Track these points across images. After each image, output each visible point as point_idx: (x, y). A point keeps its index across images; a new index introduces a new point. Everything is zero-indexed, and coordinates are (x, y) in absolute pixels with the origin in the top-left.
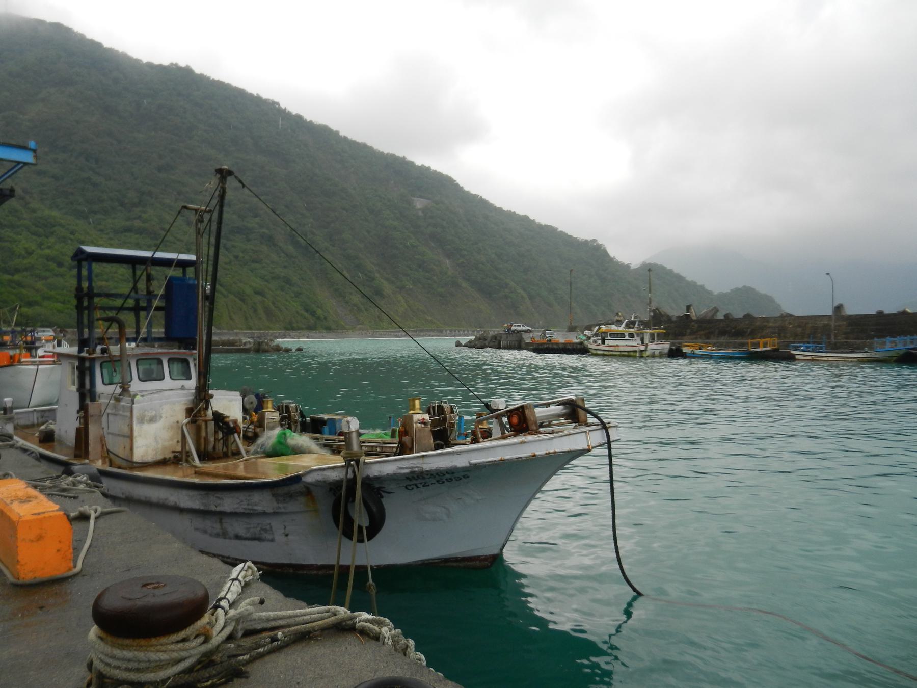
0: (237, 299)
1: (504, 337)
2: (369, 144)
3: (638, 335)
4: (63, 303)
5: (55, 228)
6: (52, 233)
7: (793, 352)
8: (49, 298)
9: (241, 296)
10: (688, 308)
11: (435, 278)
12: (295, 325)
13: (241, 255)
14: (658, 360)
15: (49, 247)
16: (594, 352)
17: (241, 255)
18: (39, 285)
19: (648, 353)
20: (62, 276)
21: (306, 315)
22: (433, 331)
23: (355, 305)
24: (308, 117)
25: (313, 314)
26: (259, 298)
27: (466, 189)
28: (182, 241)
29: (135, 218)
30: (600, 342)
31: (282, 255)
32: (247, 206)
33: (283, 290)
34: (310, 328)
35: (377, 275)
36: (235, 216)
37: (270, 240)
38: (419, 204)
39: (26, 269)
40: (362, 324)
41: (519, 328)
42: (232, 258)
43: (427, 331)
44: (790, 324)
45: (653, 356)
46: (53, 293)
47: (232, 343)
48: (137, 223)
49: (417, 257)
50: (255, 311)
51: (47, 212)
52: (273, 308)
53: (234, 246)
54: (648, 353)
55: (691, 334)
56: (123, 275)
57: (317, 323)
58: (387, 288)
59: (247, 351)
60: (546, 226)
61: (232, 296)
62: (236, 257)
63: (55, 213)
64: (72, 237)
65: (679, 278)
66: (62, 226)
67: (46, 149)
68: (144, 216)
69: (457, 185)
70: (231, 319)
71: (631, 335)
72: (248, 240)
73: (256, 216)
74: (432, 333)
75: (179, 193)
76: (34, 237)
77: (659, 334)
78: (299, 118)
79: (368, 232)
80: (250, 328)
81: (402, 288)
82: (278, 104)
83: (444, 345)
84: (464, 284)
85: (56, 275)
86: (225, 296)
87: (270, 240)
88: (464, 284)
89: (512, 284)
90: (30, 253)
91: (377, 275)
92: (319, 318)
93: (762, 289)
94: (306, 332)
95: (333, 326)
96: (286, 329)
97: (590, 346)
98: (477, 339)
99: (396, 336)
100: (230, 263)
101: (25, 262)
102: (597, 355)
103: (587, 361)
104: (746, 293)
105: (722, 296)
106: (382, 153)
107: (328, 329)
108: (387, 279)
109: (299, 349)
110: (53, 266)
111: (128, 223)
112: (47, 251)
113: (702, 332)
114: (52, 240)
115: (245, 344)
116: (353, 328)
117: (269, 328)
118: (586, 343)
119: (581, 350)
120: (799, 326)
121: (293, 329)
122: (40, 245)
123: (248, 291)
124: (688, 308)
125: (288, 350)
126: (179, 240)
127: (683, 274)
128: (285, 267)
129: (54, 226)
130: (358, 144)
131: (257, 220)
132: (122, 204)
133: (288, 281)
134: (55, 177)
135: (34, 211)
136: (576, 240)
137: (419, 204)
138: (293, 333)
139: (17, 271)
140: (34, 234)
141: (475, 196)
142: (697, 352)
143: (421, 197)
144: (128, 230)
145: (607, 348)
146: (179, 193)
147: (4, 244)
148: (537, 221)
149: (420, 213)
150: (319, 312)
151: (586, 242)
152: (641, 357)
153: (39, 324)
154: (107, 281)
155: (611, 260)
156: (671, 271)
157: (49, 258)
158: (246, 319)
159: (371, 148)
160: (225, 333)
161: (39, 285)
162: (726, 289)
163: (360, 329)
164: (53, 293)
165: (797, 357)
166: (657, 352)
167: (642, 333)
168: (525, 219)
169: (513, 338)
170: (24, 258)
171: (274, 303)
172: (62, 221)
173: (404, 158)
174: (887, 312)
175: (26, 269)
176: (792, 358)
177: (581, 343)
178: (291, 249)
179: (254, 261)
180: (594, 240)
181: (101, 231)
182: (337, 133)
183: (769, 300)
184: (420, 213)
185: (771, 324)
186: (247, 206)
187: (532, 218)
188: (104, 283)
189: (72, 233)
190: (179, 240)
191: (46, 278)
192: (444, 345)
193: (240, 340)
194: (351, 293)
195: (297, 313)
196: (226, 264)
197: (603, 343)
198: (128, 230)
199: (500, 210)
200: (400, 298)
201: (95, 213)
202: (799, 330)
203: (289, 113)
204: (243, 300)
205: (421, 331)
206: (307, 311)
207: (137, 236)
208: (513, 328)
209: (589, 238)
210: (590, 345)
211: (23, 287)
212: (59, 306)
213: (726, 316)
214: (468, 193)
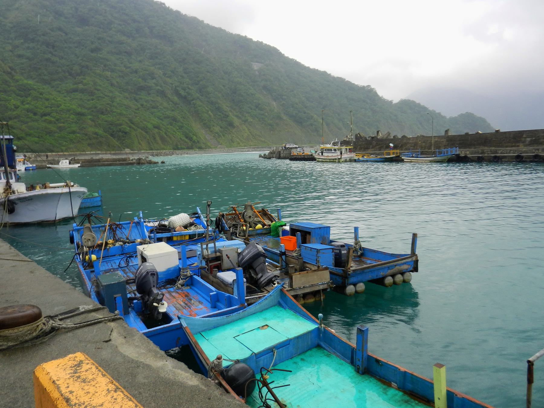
0: (143, 132)
1: (282, 152)
2: (223, 28)
3: (338, 150)
4: (38, 137)
5: (31, 91)
6: (29, 95)
7: (403, 158)
8: (30, 135)
9: (145, 129)
10: (378, 132)
11: (266, 114)
12: (179, 147)
13: (145, 104)
14: (349, 163)
15: (28, 104)
16: (318, 160)
17: (145, 104)
18: (24, 127)
19: (342, 160)
20: (37, 121)
21: (186, 140)
22: (265, 147)
23: (217, 133)
24: (183, 12)
25: (191, 139)
26: (157, 130)
27: (286, 55)
28: (108, 96)
29: (79, 83)
30: (320, 154)
31: (171, 103)
32: (147, 72)
33: (171, 125)
34: (190, 148)
35: (230, 114)
36: (140, 79)
37: (162, 94)
38: (256, 66)
39: (15, 118)
40: (221, 144)
41: (290, 146)
42: (139, 106)
43: (262, 147)
44: (420, 141)
45: (346, 161)
46: (32, 131)
47: (124, 160)
48: (81, 86)
49: (255, 101)
50: (155, 138)
51: (25, 81)
52: (166, 136)
53: (141, 99)
54: (342, 160)
55: (372, 148)
56: (73, 119)
57: (192, 144)
58: (237, 122)
59: (132, 164)
60: (338, 78)
61: (139, 130)
62: (142, 105)
63: (30, 82)
64: (41, 96)
65: (424, 109)
66: (34, 89)
67: (22, 41)
68: (85, 81)
69: (280, 53)
70: (140, 144)
71: (335, 150)
72: (149, 94)
73: (153, 79)
74: (265, 149)
75: (105, 66)
76: (19, 98)
77: (350, 149)
78: (178, 12)
79: (224, 86)
80: (152, 149)
81: (246, 121)
82: (164, 4)
83: (250, 156)
84: (285, 117)
85: (34, 121)
86: (135, 130)
87: (162, 94)
88: (285, 117)
89: (315, 116)
90: (17, 107)
91: (230, 114)
92: (194, 142)
93: (478, 114)
94: (185, 151)
95: (203, 146)
96: (174, 149)
97: (316, 157)
98: (271, 153)
99: (242, 151)
100: (138, 109)
101: (14, 113)
102: (319, 161)
103: (318, 167)
104: (468, 117)
105: (454, 120)
106: (232, 34)
107: (200, 148)
108: (237, 116)
109: (163, 162)
110: (31, 115)
111: (75, 86)
112: (27, 106)
113: (378, 147)
114: (29, 99)
115: (132, 160)
116: (216, 148)
117: (163, 149)
118: (314, 155)
119: (311, 158)
120: (424, 142)
121: (178, 149)
122: (22, 102)
123: (150, 126)
124: (378, 132)
125: (155, 163)
126: (106, 96)
127: (426, 105)
128: (173, 110)
129: (30, 90)
130: (216, 28)
131: (154, 81)
132: (71, 74)
133: (175, 119)
134: (28, 58)
135: (17, 81)
136: (357, 86)
137: (256, 66)
138: (177, 152)
139: (10, 119)
140: (18, 95)
141: (292, 60)
142: (361, 159)
143: (257, 62)
144: (75, 90)
145: (323, 158)
146: (105, 66)
147: (1, 102)
148: (332, 75)
149: (257, 73)
150: (194, 138)
151: (363, 87)
152: (339, 162)
153: (25, 150)
154: (64, 123)
155: (380, 99)
156: (419, 104)
157: (28, 110)
158: (149, 143)
159: (224, 31)
160: (99, 154)
161: (24, 127)
162: (455, 115)
163: (220, 148)
164: (32, 131)
165: (405, 160)
166: (348, 159)
167: (341, 149)
168: (324, 73)
169: (286, 152)
170: (14, 111)
171: (166, 133)
172: (35, 87)
173: (246, 36)
174: (502, 130)
175: (15, 118)
176: (402, 161)
177: (312, 155)
178: (176, 99)
179: (153, 108)
180: (369, 86)
181: (59, 92)
182: (203, 21)
183: (484, 120)
184: (257, 73)
185: (411, 141)
186: (147, 72)
187: (329, 73)
188: (62, 124)
189: (41, 94)
190: (106, 96)
191: (27, 123)
192: (250, 156)
193: (129, 158)
194: (214, 126)
195: (181, 139)
196: (136, 109)
197: (322, 154)
198: (75, 90)
199: (308, 69)
200: (244, 127)
201: (55, 80)
202: (424, 144)
203: (171, 10)
204: (147, 132)
205: (258, 148)
206: (187, 138)
207: (80, 94)
208: (287, 146)
209: (366, 85)
210: (316, 156)
211: (14, 128)
212: (36, 139)
213: (394, 137)
214: (287, 58)
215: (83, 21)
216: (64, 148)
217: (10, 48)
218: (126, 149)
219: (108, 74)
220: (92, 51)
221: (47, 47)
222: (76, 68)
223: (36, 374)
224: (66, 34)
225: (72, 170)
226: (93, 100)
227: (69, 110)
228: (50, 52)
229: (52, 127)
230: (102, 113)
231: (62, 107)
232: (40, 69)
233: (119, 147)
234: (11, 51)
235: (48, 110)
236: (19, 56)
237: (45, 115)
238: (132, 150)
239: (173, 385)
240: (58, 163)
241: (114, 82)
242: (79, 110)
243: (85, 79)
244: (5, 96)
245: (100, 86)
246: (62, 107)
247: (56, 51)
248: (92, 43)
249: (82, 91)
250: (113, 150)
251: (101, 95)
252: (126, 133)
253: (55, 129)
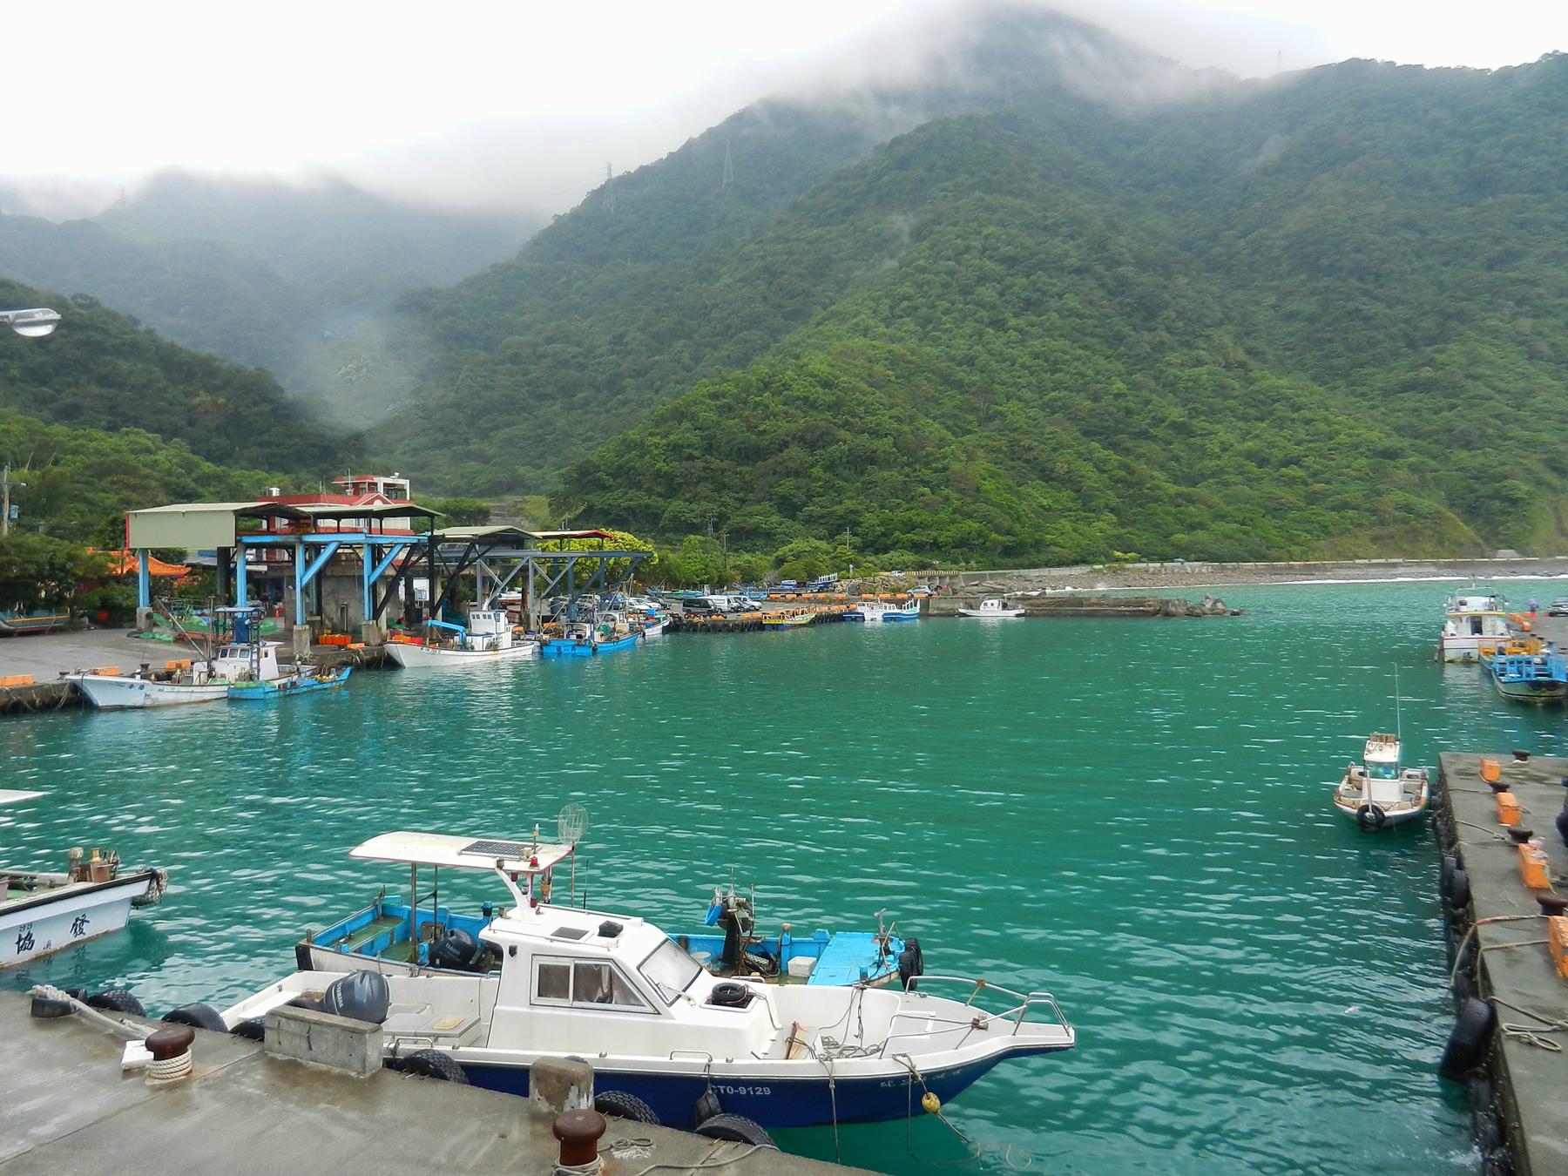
8: (1223, 517)
39: (1213, 474)
46: (1230, 509)
48: (1427, 372)
67: (1303, 277)
68: (1441, 358)
110: (1251, 466)
126: (1500, 392)
146: (1519, 303)
164: (1230, 509)
190: (1500, 392)
215: (1480, 185)
216: (1295, 549)
217: (1272, 300)
218: (1502, 552)
219: (1525, 324)
220: (1491, 266)
221: (1361, 280)
222: (1428, 323)
223: (640, 919)
224: (1423, 233)
225: (1005, 624)
226: (1452, 407)
227: (1356, 447)
228: (1366, 293)
229: (1287, 495)
230: (1467, 445)
231: (1342, 438)
232: (1330, 341)
233: (1476, 545)
234: (1273, 307)
235: (1296, 451)
236: (1290, 317)
237: (1286, 464)
238: (1523, 553)
239: (487, 912)
240: (887, 618)
241: (1542, 346)
242: (1388, 443)
243: (1441, 351)
244: (1206, 425)
245: (1491, 363)
246: (1342, 438)
247: (1382, 286)
248: (1497, 241)
249: (1427, 387)
250: (1453, 554)
251: (1484, 391)
252: (1514, 502)
253: (1293, 499)
